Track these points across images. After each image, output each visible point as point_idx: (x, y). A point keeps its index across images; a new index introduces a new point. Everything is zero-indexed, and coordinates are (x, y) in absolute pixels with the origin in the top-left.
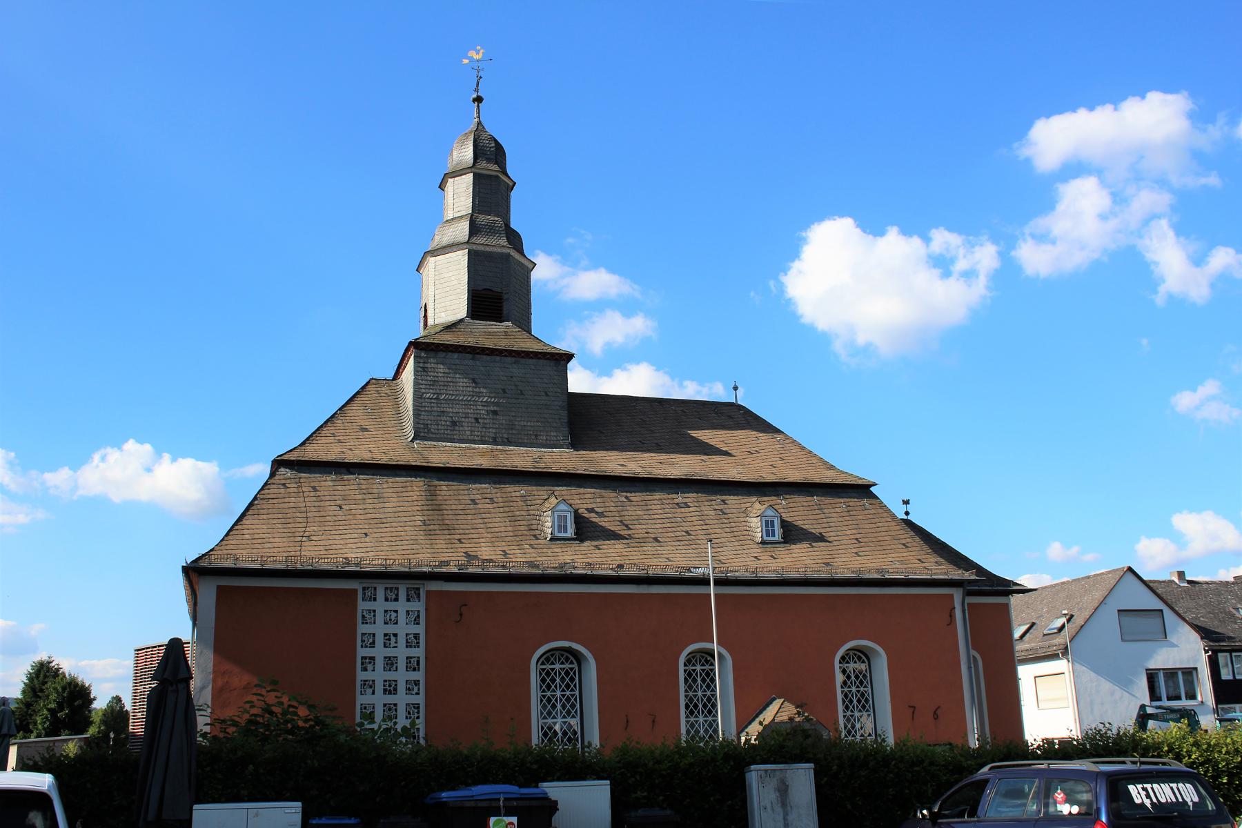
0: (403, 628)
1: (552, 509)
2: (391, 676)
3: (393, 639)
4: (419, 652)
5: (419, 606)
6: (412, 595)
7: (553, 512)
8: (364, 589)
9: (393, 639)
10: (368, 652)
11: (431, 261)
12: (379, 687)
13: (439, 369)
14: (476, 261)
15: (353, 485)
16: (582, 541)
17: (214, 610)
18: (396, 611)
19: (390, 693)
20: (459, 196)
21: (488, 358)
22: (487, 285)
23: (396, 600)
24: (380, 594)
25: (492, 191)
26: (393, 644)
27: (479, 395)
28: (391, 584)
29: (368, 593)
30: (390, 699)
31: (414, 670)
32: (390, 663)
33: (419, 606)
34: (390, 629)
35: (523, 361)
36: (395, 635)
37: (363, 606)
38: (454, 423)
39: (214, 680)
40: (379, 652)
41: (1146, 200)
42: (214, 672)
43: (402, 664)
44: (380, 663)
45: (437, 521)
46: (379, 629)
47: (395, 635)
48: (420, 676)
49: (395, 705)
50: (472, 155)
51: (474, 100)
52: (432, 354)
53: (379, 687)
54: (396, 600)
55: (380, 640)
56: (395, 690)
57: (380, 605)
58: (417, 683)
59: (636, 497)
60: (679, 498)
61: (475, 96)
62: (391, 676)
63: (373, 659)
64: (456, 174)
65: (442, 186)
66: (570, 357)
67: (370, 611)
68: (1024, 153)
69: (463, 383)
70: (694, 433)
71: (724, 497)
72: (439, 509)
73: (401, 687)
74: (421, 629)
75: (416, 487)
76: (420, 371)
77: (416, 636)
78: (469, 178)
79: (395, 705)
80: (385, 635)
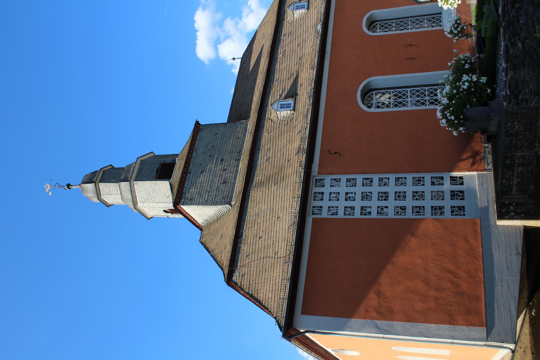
0: (342, 189)
1: (278, 113)
2: (375, 196)
3: (349, 195)
4: (360, 178)
5: (328, 179)
6: (320, 183)
7: (278, 111)
8: (313, 214)
9: (349, 195)
10: (357, 211)
11: (140, 205)
12: (383, 203)
13: (192, 191)
14: (140, 177)
15: (248, 233)
16: (297, 95)
17: (319, 317)
18: (331, 193)
19: (388, 197)
20: (112, 193)
21: (191, 165)
22: (155, 171)
23: (322, 193)
24: (318, 203)
25: (112, 175)
26: (353, 195)
27: (210, 169)
28: (311, 196)
29: (316, 211)
30: (392, 196)
31: (372, 181)
32: (366, 196)
33: (328, 179)
34: (342, 197)
35: (196, 147)
36: (347, 194)
37: (325, 214)
38: (224, 182)
39: (372, 318)
40: (358, 204)
41: (229, 25)
42: (365, 318)
43: (367, 189)
44: (366, 203)
45: (277, 178)
46: (342, 204)
47: (347, 194)
48: (376, 178)
49: (396, 193)
50: (91, 184)
51: (68, 188)
52: (183, 195)
53: (383, 203)
54: (322, 193)
55: (350, 204)
56: (385, 193)
57: (325, 204)
58: (381, 180)
59: (276, 76)
60: (280, 56)
61: (66, 188)
62: (375, 196)
63: (362, 208)
64: (98, 194)
65: (108, 206)
66: (197, 123)
67: (329, 211)
68: (207, 62)
69: (202, 178)
70: (251, 68)
71: (283, 35)
72: (269, 178)
73: (384, 189)
74: (344, 178)
75: (255, 194)
76: (191, 202)
77: (348, 180)
78: (102, 186)
79: (396, 193)
80: (346, 200)
